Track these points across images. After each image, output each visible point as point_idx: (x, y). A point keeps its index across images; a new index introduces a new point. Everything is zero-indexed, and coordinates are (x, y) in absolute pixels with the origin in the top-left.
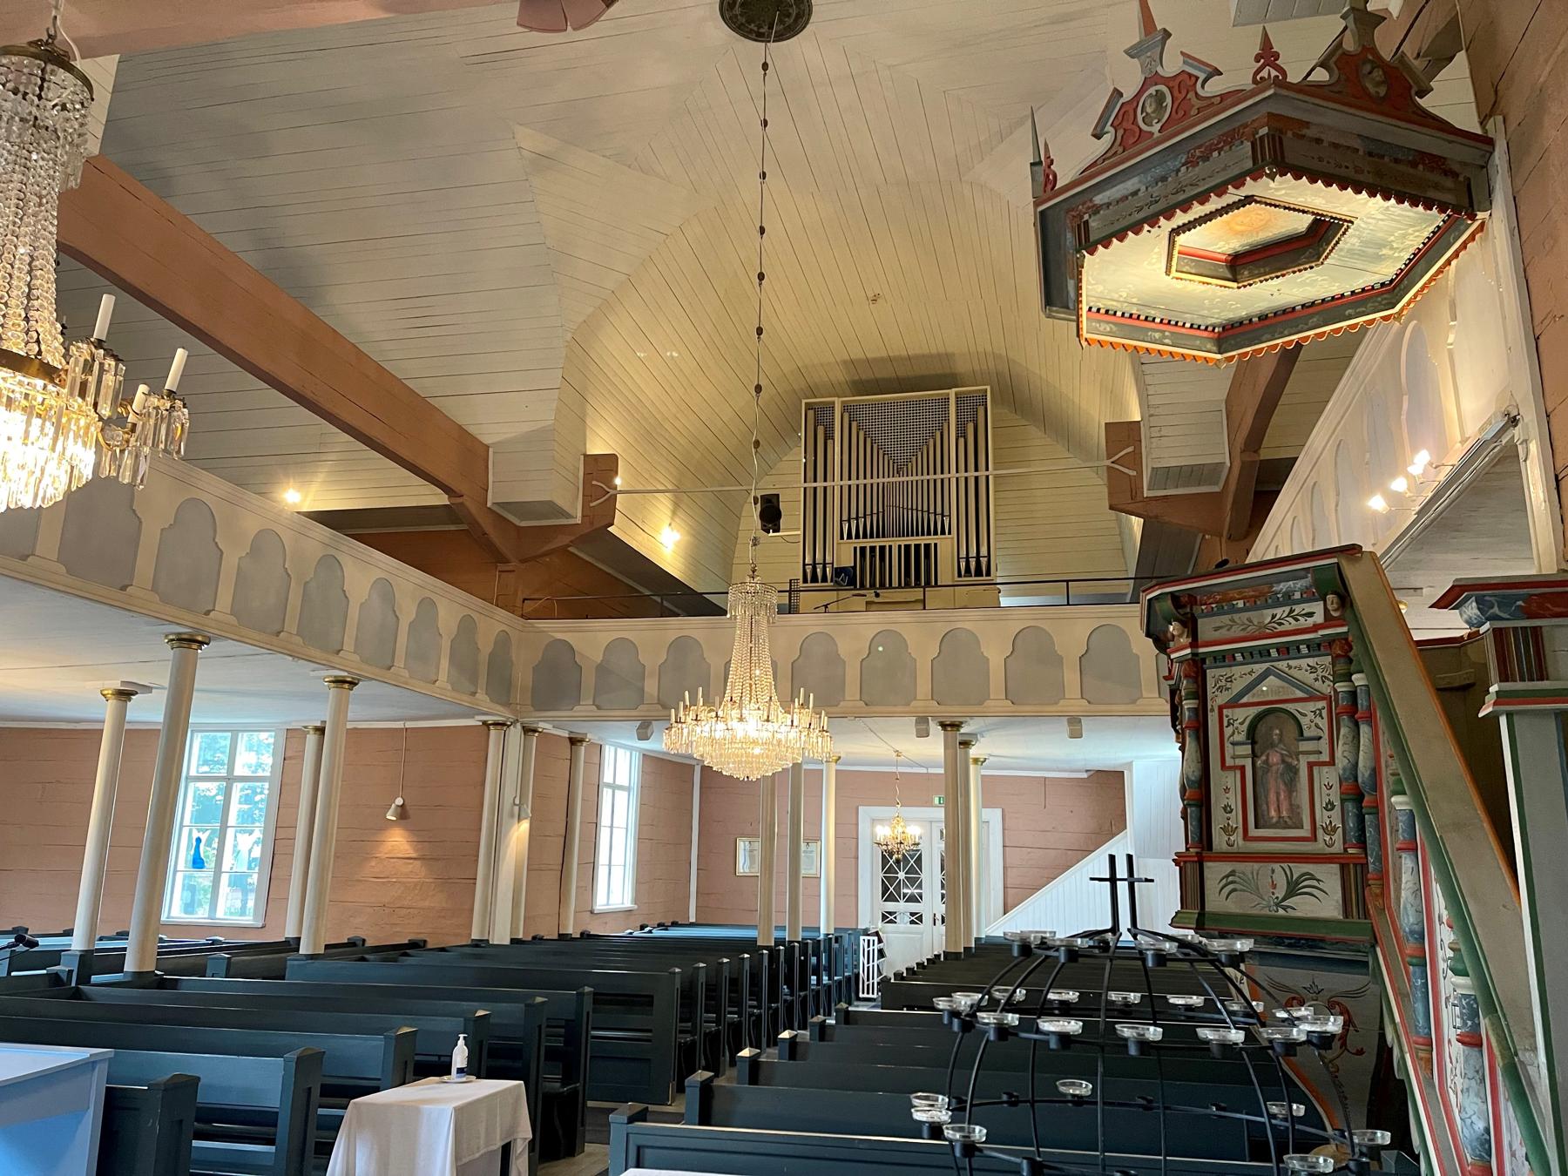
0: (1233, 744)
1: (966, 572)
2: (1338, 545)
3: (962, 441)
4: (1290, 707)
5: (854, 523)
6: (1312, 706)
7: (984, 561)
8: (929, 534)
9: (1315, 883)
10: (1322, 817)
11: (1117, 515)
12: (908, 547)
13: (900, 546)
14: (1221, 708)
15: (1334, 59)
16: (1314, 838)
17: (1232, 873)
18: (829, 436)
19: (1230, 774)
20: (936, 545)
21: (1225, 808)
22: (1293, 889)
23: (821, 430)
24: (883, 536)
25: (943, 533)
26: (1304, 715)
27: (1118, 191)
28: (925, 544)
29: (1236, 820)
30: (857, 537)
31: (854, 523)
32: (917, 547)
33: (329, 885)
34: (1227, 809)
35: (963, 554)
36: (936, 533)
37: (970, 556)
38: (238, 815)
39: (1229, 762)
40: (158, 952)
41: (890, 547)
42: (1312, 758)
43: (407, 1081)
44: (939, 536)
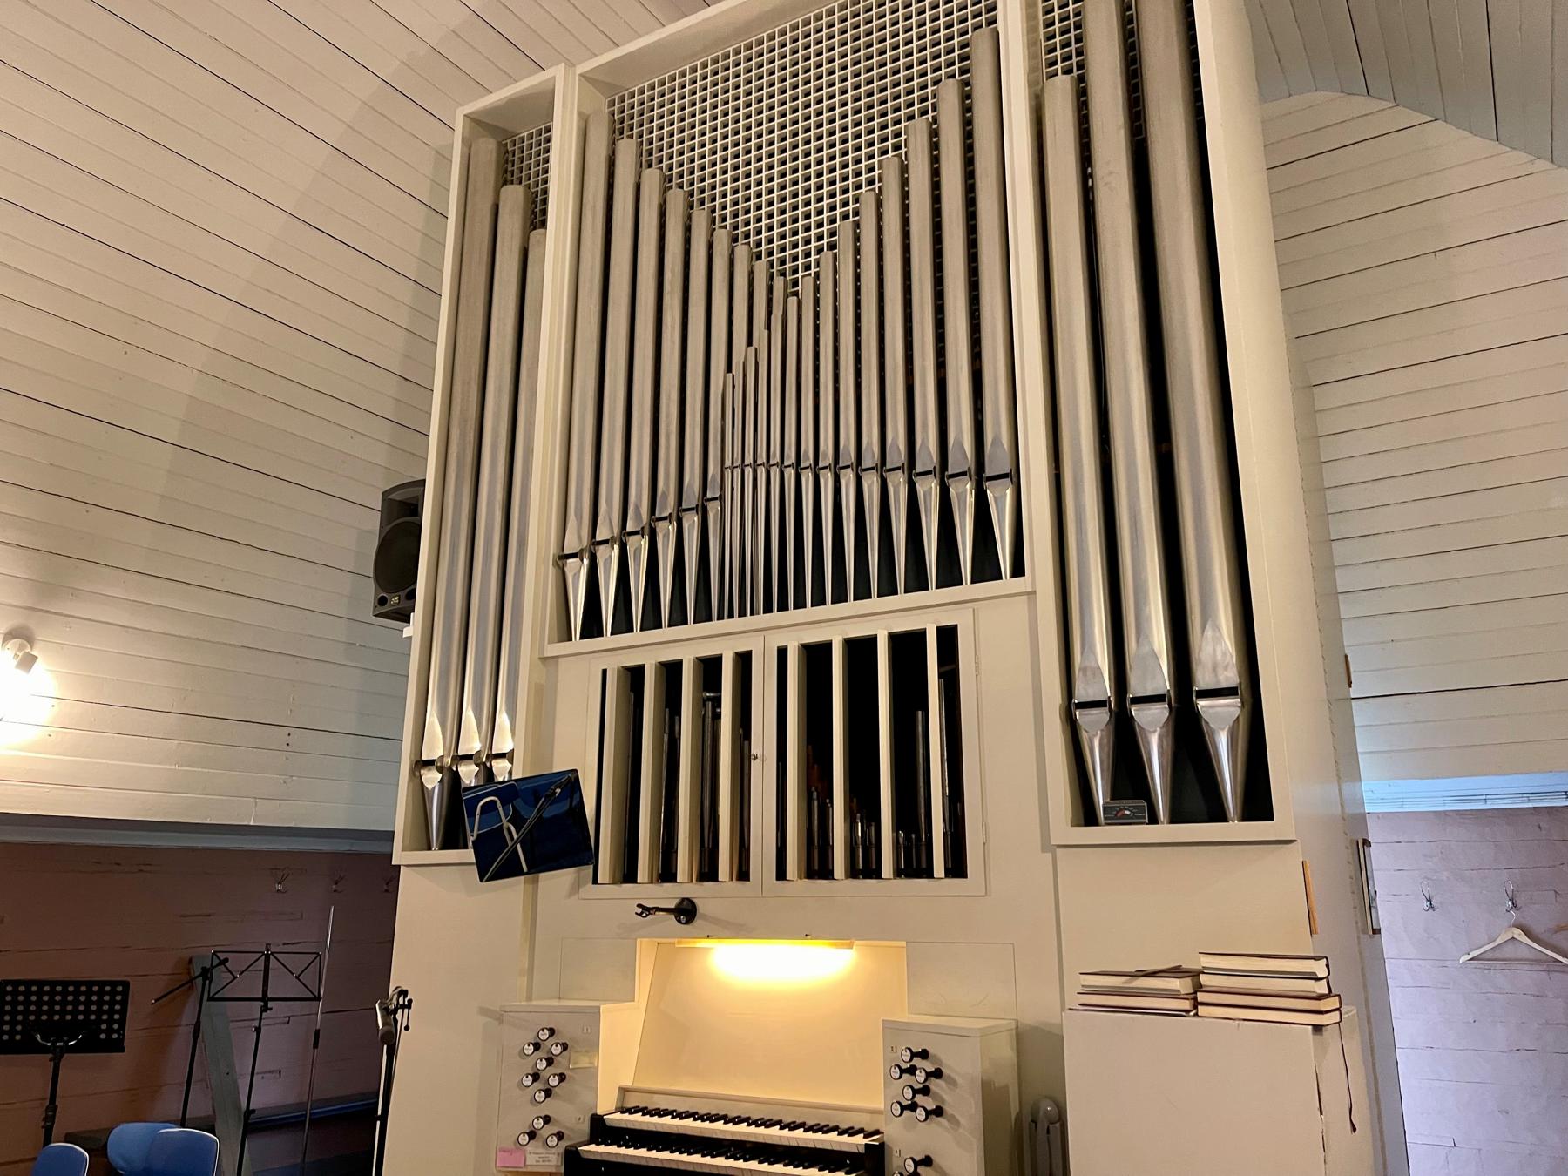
1: (1116, 792)
2: (57, 1094)
3: (1060, 91)
5: (609, 559)
7: (1220, 717)
8: (918, 582)
11: (258, 1073)
12: (817, 656)
13: (782, 653)
18: (536, 217)
20: (948, 636)
23: (513, 197)
24: (703, 615)
25: (986, 568)
27: (673, 272)
28: (894, 639)
30: (623, 624)
31: (609, 559)
32: (860, 650)
33: (816, 834)
35: (1097, 682)
36: (950, 577)
37: (1136, 688)
40: (853, 873)
41: (744, 661)
43: (442, 241)
44: (968, 590)
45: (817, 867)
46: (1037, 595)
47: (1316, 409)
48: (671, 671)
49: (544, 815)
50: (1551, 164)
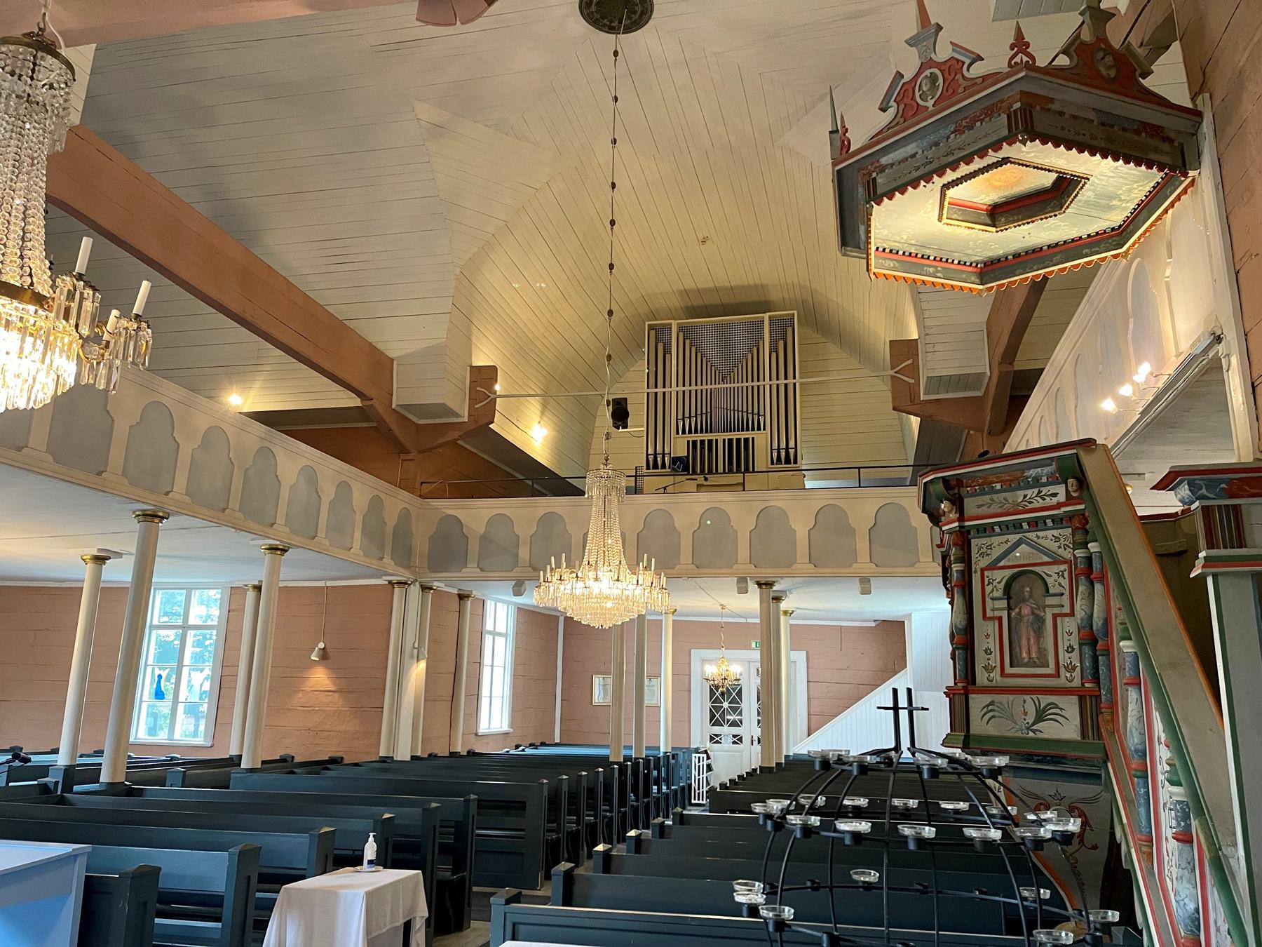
0: (993, 599)
1: (777, 461)
3: (774, 355)
4: (1038, 569)
5: (687, 422)
6: (1056, 568)
7: (792, 452)
8: (748, 430)
9: (1058, 711)
10: (1064, 658)
11: (899, 415)
12: (730, 441)
13: (724, 440)
14: (983, 570)
15: (1074, 48)
16: (1058, 675)
17: (992, 703)
18: (667, 351)
19: (990, 623)
20: (753, 439)
21: (986, 651)
22: (1041, 716)
23: (660, 346)
24: (711, 432)
25: (759, 429)
26: (1050, 576)
28: (744, 438)
29: (995, 660)
30: (690, 432)
31: (687, 422)
32: (738, 440)
34: (988, 652)
35: (775, 446)
36: (753, 429)
37: (781, 447)
38: (192, 657)
39: (989, 614)
41: (717, 440)
42: (1056, 611)
44: (756, 432)
45: (128, 768)
46: (156, 898)
47: (496, 637)
48: (730, 383)
49: (666, 822)
50: (1189, 100)
